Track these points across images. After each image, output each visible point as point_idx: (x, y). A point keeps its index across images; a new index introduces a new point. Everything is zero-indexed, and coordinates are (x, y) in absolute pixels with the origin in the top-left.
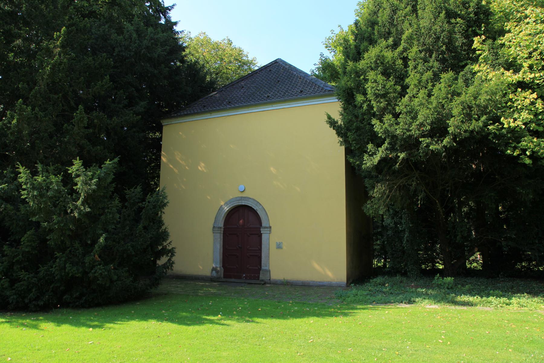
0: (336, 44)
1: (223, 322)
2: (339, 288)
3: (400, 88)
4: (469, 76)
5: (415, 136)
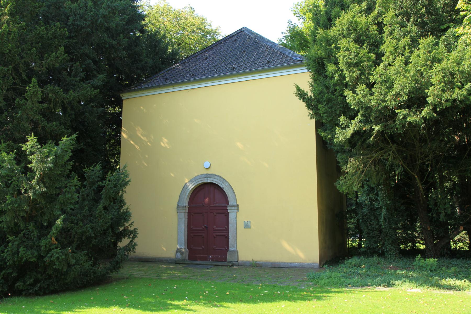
0: (305, 11)
1: (189, 307)
2: (312, 270)
3: (374, 55)
4: (451, 40)
5: (391, 106)
